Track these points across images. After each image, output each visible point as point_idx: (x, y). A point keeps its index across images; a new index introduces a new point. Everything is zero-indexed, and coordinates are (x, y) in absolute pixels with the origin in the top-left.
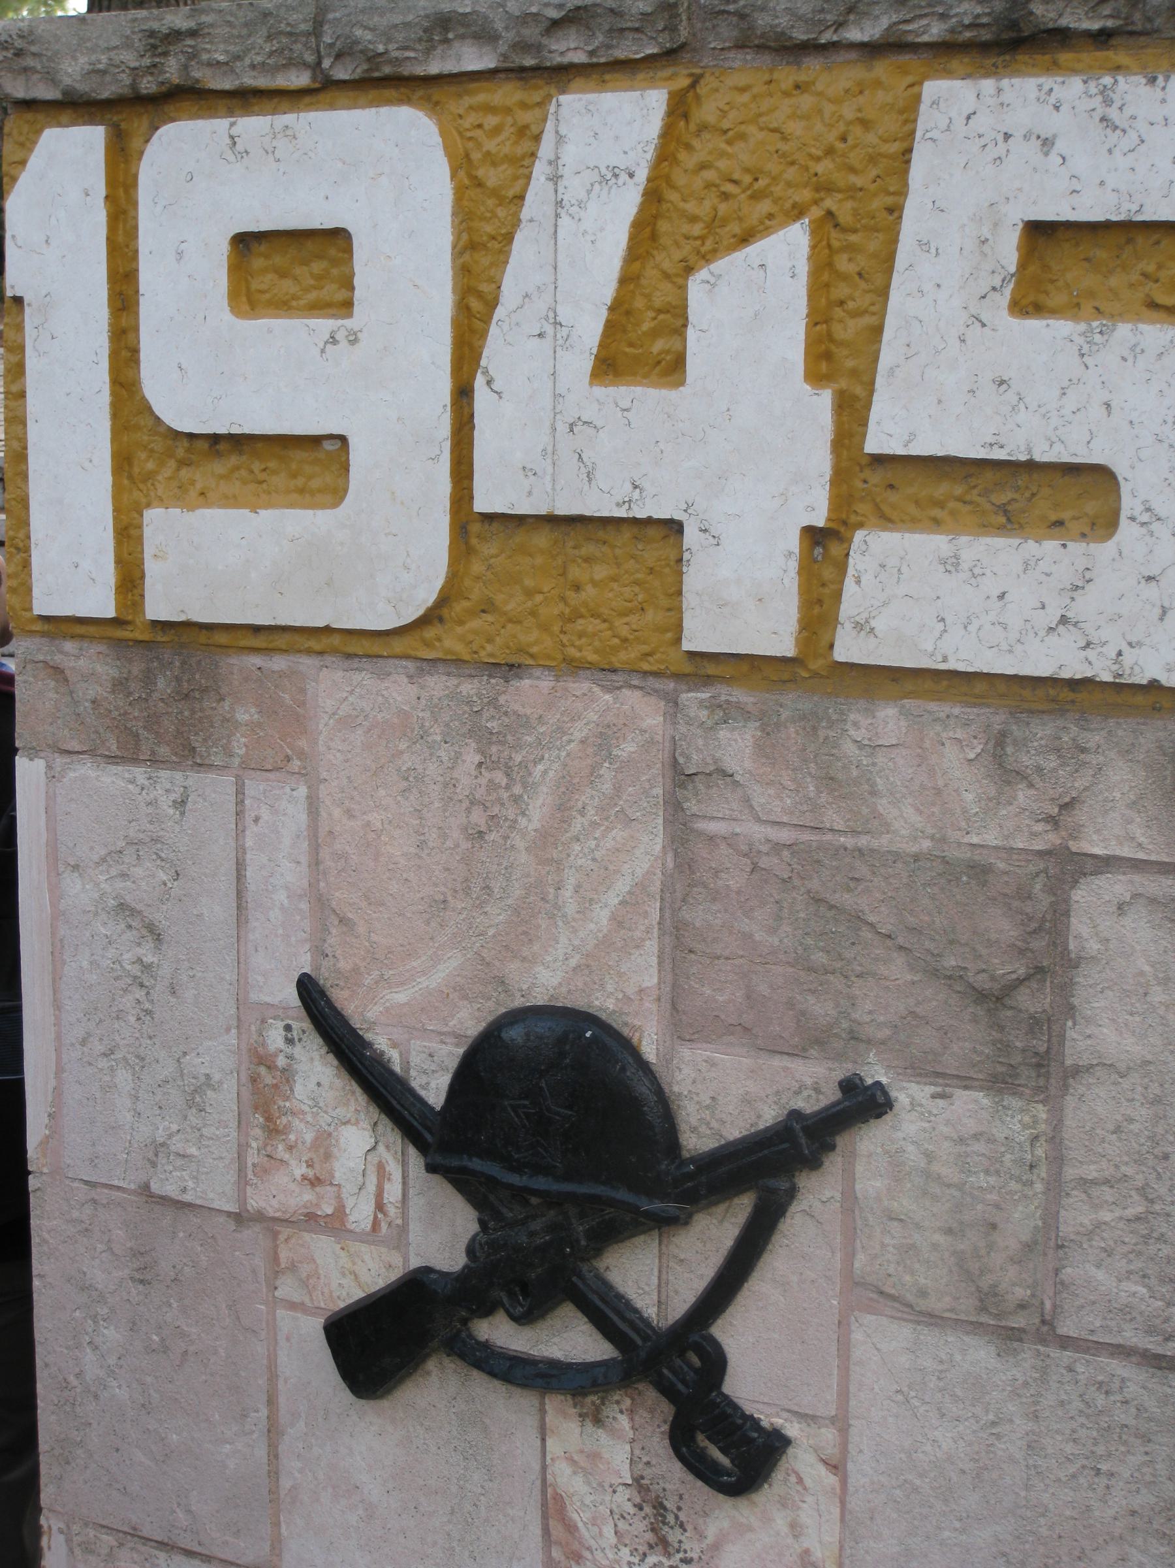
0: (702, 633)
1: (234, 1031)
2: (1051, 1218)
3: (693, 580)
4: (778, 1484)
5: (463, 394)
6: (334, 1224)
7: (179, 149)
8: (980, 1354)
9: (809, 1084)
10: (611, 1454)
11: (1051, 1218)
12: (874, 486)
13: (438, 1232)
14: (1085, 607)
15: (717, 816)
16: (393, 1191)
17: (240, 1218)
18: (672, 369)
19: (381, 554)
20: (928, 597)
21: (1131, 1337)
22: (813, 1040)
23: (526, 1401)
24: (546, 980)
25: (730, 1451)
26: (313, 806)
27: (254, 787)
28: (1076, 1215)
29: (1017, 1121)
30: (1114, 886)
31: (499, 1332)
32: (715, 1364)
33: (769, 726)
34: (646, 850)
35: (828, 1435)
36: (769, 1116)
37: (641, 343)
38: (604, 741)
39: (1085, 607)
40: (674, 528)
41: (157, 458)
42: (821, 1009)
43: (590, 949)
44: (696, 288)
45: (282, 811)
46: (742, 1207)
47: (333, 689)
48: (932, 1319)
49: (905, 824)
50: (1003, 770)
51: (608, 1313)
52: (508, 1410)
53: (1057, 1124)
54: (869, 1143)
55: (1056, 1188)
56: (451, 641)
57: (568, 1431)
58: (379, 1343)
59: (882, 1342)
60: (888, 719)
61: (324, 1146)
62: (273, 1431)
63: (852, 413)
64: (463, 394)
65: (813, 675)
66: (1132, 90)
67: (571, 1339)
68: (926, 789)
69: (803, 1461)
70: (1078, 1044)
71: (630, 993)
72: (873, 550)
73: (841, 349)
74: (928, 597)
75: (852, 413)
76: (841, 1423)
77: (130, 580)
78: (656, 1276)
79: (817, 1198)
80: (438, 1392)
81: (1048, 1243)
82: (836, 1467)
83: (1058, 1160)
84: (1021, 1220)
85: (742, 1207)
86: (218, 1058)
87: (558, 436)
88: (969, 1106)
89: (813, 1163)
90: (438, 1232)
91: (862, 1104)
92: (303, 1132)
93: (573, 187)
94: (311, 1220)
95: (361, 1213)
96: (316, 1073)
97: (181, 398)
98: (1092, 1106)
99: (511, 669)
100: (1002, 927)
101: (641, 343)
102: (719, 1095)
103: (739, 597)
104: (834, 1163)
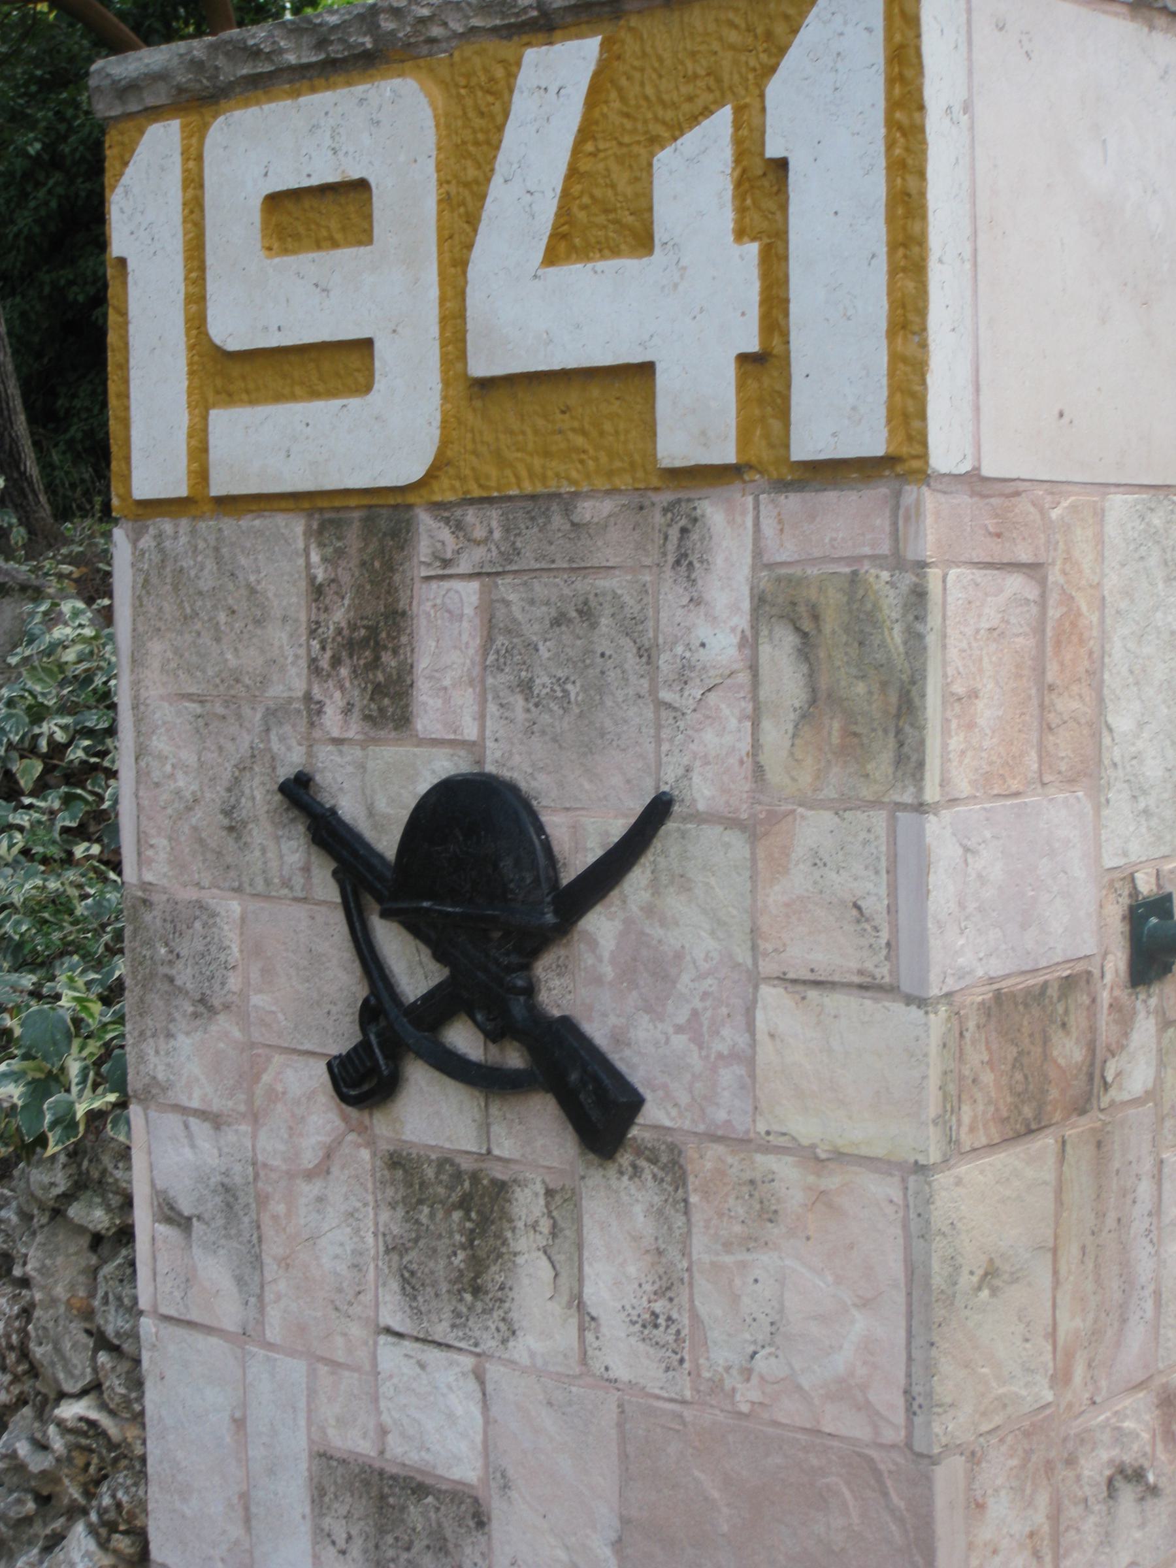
26: (197, 322)
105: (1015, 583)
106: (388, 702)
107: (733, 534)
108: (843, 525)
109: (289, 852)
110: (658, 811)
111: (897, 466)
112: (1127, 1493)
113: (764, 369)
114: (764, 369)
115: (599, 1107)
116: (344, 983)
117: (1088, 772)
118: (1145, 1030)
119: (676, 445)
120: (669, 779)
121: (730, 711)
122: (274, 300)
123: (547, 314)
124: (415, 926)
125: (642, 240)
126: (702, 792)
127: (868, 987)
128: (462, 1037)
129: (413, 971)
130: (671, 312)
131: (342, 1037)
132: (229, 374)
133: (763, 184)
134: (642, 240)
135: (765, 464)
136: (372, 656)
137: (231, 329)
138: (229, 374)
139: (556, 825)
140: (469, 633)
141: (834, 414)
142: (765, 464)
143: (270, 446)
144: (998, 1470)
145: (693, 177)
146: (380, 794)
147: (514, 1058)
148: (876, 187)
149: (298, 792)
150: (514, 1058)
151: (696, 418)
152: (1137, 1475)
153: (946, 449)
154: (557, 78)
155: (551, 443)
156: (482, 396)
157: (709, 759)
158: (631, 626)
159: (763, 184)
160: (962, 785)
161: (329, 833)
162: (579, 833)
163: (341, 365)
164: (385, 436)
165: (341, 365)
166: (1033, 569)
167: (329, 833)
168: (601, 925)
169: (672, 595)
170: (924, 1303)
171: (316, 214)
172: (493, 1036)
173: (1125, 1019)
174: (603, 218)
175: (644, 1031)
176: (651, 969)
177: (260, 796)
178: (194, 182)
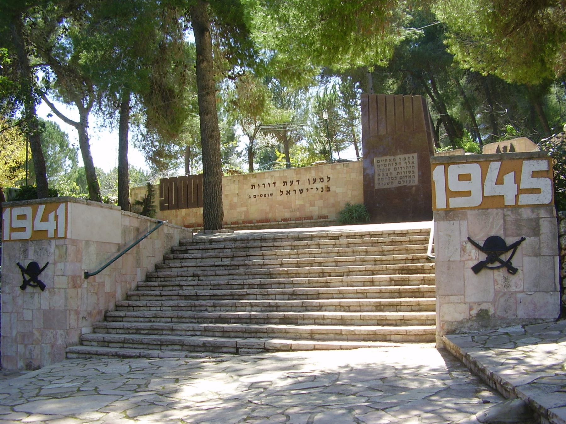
0: (506, 204)
1: (217, 397)
2: (540, 246)
3: (505, 200)
4: (517, 273)
5: (483, 187)
6: (471, 259)
7: (452, 168)
8: (535, 258)
9: (518, 239)
10: (503, 272)
11: (540, 246)
12: (521, 191)
13: (483, 257)
14: (539, 199)
15: (508, 218)
16: (478, 255)
17: (460, 261)
18: (502, 183)
19: (476, 200)
20: (525, 199)
21: (547, 254)
22: (518, 235)
23: (492, 271)
24: (493, 234)
25: (513, 271)
26: (468, 222)
27: (461, 222)
28: (542, 245)
29: (536, 239)
30: (543, 219)
31: (490, 265)
32: (511, 263)
33: (512, 211)
34: (501, 222)
35: (521, 268)
36: (514, 242)
37: (499, 181)
38: (497, 214)
39: (539, 199)
40: (503, 196)
41: (450, 194)
42: (519, 232)
43: (497, 231)
44: (504, 177)
45: (464, 223)
46: (512, 250)
47: (469, 212)
48: (530, 256)
49: (525, 216)
50: (533, 212)
51: (501, 261)
52: (490, 272)
53: (539, 239)
54: (524, 242)
55: (540, 243)
56: (482, 207)
57: (496, 272)
58: (477, 269)
59: (526, 259)
60: (523, 209)
61: (470, 252)
62: (464, 280)
63: (518, 186)
64: (483, 187)
65: (516, 207)
66: (540, 161)
67: (497, 264)
68: (526, 214)
69: (520, 271)
70: (541, 232)
71: (501, 234)
72: (521, 196)
73: (517, 181)
74: (525, 199)
75: (518, 186)
76: (523, 267)
77: (448, 205)
78: (504, 257)
79: (519, 248)
80: (483, 272)
81: (540, 248)
82: (522, 270)
83: (540, 241)
84: (537, 247)
85: (512, 250)
86: (458, 247)
87: (491, 189)
88: (532, 238)
89: (519, 245)
90: (483, 257)
91: (523, 239)
92: (468, 251)
93: (493, 170)
94: (469, 260)
95: (474, 258)
96: (469, 246)
97: (452, 188)
98: (542, 237)
99: (487, 209)
100: (534, 224)
101: (499, 181)
102: (510, 241)
103: (510, 201)
104: (521, 245)
105: (74, 247)
106: (26, 257)
107: (53, 242)
108: (61, 242)
109: (18, 268)
110: (48, 263)
111: (65, 238)
112: (84, 319)
113: (56, 231)
114: (56, 231)
115: (42, 287)
116: (22, 280)
117: (81, 261)
118: (86, 282)
119: (50, 236)
120: (48, 261)
121: (53, 256)
122: (17, 224)
123: (40, 226)
124: (28, 274)
125: (48, 221)
126: (50, 262)
127: (62, 275)
128: (32, 283)
129: (27, 277)
130: (50, 226)
131: (21, 284)
132: (13, 230)
133: (56, 217)
134: (48, 221)
135: (56, 237)
136: (25, 251)
137: (14, 226)
138: (13, 230)
139: (40, 265)
140: (33, 250)
141: (61, 234)
142: (56, 237)
143: (16, 236)
144: (72, 313)
145: (52, 216)
146: (25, 264)
147: (36, 284)
148: (64, 218)
149: (18, 264)
150: (36, 284)
151: (51, 234)
152: (85, 318)
153: (69, 236)
154: (42, 208)
155: (40, 236)
156: (36, 233)
157: (51, 260)
158: (46, 250)
159: (56, 217)
160: (69, 260)
161: (21, 267)
162: (41, 266)
163: (23, 229)
164: (27, 235)
165: (23, 229)
166: (76, 246)
167: (21, 267)
168: (43, 273)
169: (49, 247)
170: (66, 299)
171: (22, 217)
172: (34, 282)
173: (84, 281)
174: (45, 219)
175: (46, 280)
176: (47, 276)
177: (14, 265)
178: (11, 214)
